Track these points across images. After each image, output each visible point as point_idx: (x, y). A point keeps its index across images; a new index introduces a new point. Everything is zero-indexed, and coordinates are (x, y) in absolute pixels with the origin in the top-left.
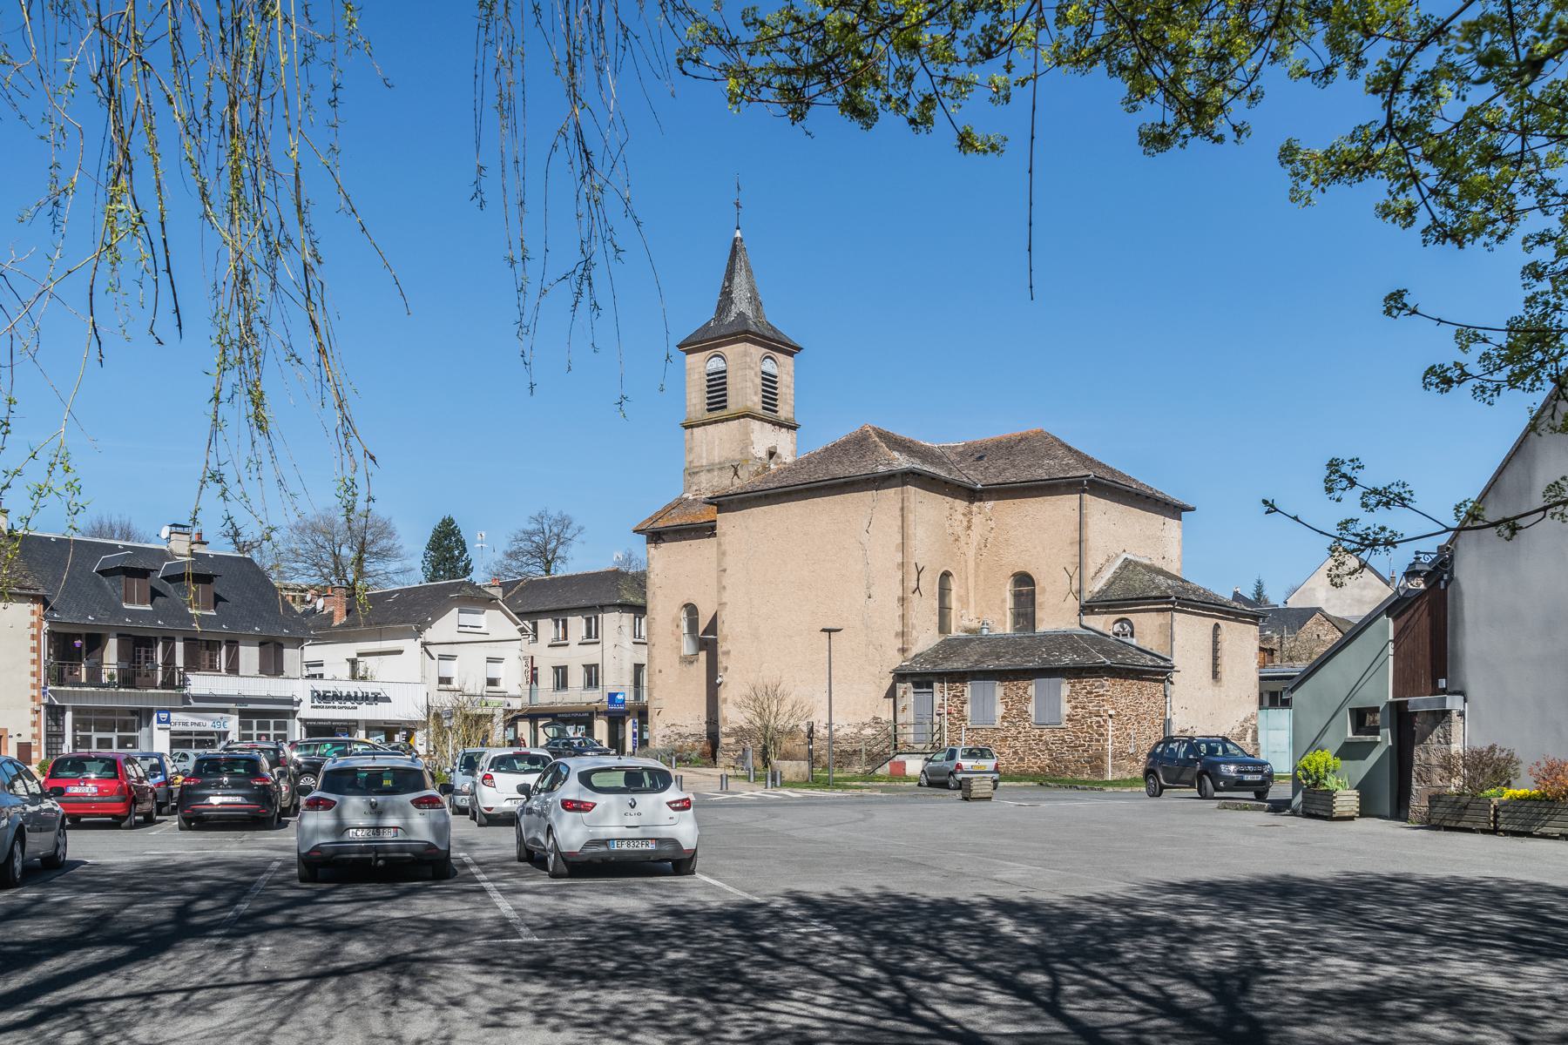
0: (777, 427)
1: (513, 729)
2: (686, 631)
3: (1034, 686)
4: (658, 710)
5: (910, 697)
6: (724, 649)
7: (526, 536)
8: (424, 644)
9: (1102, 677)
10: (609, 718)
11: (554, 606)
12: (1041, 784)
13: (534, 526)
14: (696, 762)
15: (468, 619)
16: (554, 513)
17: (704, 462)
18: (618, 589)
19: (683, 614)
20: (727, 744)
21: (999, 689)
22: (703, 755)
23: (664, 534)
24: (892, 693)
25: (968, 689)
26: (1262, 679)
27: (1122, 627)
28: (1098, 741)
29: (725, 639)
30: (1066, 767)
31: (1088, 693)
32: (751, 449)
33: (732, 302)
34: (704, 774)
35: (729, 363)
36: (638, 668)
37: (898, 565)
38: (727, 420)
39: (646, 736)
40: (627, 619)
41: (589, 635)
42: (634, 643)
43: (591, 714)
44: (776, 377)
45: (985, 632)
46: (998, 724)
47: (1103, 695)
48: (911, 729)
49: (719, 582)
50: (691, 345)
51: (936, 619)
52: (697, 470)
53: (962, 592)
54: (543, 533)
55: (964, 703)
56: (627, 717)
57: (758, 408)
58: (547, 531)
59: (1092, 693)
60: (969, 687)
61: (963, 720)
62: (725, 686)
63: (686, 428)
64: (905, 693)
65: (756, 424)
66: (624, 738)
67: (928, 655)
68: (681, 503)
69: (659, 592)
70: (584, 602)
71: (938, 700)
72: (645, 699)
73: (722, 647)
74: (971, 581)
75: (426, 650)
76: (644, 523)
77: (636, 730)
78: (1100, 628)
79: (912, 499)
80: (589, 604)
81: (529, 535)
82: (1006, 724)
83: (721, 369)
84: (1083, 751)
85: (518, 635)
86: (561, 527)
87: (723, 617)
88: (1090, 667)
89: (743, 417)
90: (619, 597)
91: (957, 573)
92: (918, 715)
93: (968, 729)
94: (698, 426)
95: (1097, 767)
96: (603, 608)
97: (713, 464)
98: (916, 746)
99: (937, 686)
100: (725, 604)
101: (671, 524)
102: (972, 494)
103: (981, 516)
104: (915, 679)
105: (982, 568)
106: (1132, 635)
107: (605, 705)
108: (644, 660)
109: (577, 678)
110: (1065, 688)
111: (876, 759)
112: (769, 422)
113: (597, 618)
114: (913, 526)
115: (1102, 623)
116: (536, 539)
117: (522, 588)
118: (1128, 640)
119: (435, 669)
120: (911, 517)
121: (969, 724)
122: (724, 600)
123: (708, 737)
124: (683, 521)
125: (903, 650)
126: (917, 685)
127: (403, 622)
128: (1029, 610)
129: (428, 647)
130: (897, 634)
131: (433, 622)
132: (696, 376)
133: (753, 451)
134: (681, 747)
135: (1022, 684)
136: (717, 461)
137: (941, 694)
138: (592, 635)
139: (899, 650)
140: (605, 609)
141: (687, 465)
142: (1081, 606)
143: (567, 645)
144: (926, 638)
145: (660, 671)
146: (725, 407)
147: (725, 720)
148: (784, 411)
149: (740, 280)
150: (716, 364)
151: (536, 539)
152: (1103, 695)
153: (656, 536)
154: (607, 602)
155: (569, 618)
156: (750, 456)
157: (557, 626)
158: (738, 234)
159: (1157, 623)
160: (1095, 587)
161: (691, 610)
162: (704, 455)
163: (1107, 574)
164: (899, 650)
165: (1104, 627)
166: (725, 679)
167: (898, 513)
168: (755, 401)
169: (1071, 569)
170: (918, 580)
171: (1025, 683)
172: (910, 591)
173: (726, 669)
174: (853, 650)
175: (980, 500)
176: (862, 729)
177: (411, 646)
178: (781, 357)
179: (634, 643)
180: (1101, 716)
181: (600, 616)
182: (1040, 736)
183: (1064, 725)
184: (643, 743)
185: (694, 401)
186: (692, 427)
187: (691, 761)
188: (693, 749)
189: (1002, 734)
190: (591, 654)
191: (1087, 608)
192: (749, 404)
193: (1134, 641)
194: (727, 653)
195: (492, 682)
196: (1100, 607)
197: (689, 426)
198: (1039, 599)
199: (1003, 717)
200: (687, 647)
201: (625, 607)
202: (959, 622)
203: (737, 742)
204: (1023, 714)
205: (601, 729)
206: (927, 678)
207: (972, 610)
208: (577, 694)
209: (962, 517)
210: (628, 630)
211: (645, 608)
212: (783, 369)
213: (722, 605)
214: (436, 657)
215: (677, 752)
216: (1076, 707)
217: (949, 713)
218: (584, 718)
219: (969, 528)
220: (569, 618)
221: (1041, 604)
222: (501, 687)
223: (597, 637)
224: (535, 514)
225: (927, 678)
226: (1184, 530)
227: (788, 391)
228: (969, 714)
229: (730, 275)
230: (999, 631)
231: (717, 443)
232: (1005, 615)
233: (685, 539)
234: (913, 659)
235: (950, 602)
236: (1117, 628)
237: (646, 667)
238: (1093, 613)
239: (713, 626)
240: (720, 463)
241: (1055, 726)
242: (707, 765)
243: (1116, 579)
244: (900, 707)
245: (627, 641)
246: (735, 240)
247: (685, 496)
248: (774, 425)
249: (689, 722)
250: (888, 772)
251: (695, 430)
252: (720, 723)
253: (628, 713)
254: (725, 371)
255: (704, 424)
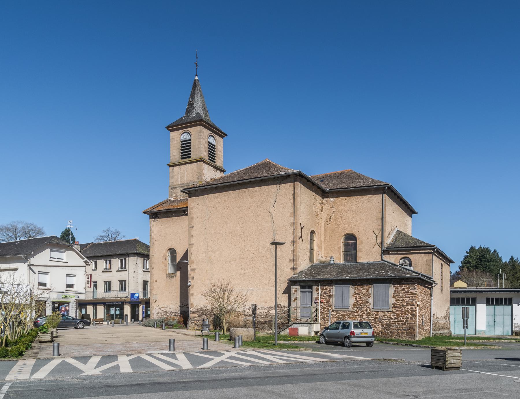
0: (215, 169)
1: (85, 309)
2: (170, 262)
3: (373, 288)
4: (155, 300)
5: (299, 293)
6: (192, 268)
7: (101, 238)
8: (30, 266)
9: (415, 284)
10: (131, 305)
11: (105, 254)
12: (382, 342)
13: (105, 234)
14: (176, 326)
15: (54, 254)
16: (113, 230)
17: (179, 183)
18: (136, 247)
19: (169, 254)
20: (193, 317)
21: (352, 290)
22: (179, 322)
23: (159, 214)
24: (287, 291)
25: (333, 290)
26: (451, 291)
27: (404, 261)
28: (412, 319)
29: (193, 262)
30: (392, 333)
31: (406, 292)
32: (203, 177)
33: (194, 108)
34: (182, 334)
35: (192, 136)
36: (145, 283)
37: (291, 223)
38: (191, 163)
39: (149, 313)
40: (140, 260)
41: (122, 267)
42: (144, 271)
43: (122, 303)
44: (215, 146)
45: (332, 262)
46: (351, 308)
47: (415, 294)
48: (299, 311)
49: (190, 233)
50: (172, 127)
51: (308, 254)
52: (176, 186)
53: (319, 243)
54: (109, 237)
55: (330, 297)
56: (140, 304)
57: (207, 158)
58: (110, 236)
59: (408, 292)
60: (334, 288)
61: (330, 306)
62: (193, 287)
63: (170, 166)
64: (296, 291)
65: (205, 166)
66: (138, 314)
67: (305, 272)
68: (167, 201)
69: (156, 243)
70: (119, 252)
71: (315, 295)
72: (149, 296)
73: (191, 267)
74: (323, 237)
75: (31, 269)
76: (149, 209)
77: (144, 310)
78: (392, 261)
79: (299, 189)
80: (122, 253)
81: (103, 237)
82: (355, 309)
83: (188, 139)
84: (402, 324)
85: (84, 264)
86: (116, 235)
87: (192, 251)
88: (407, 278)
89: (199, 161)
90: (136, 250)
91: (317, 232)
92: (302, 303)
93: (333, 311)
94: (176, 165)
95: (411, 333)
96: (128, 255)
97: (184, 184)
98: (302, 320)
99: (314, 287)
100: (193, 244)
101: (162, 209)
102: (324, 194)
103: (328, 205)
104: (302, 284)
105: (328, 231)
106: (410, 265)
107: (129, 299)
108: (148, 279)
109: (115, 286)
110: (392, 290)
111: (281, 327)
112: (212, 166)
113: (125, 260)
114: (299, 204)
115: (394, 259)
116: (106, 239)
117: (90, 247)
118: (408, 268)
119: (35, 279)
120: (298, 199)
121: (333, 308)
122: (192, 242)
123: (180, 314)
124: (169, 208)
125: (294, 269)
126: (302, 287)
127: (18, 254)
128: (353, 253)
129: (32, 267)
130: (290, 260)
131: (35, 254)
132: (175, 142)
133: (204, 178)
134: (167, 318)
135: (366, 287)
136: (186, 182)
137: (317, 292)
138: (123, 267)
139: (291, 269)
140: (130, 255)
141: (170, 184)
142: (382, 251)
143: (111, 271)
144: (304, 265)
145: (156, 281)
146: (190, 157)
147: (192, 304)
148: (219, 162)
149: (198, 99)
150: (186, 137)
151: (106, 239)
152: (415, 294)
153: (154, 215)
154: (130, 252)
155: (112, 259)
156: (202, 180)
157: (106, 263)
158: (197, 78)
159: (425, 260)
160: (388, 241)
161: (173, 251)
162: (179, 180)
163: (392, 236)
164: (291, 269)
165: (395, 261)
166: (192, 283)
167: (292, 196)
168: (205, 155)
169: (377, 232)
170: (301, 232)
171: (367, 287)
172: (298, 238)
173: (193, 278)
174: (265, 268)
175: (327, 197)
176: (269, 310)
177: (22, 267)
178: (217, 137)
179: (144, 271)
180: (414, 305)
181: (127, 258)
182: (376, 315)
183: (391, 309)
184: (147, 316)
185: (174, 154)
186: (173, 166)
187: (173, 325)
188: (174, 319)
189: (353, 314)
190: (123, 276)
191: (385, 252)
192: (202, 155)
193: (412, 268)
194: (194, 270)
195: (70, 286)
196: (393, 251)
197: (172, 166)
198: (359, 247)
199: (353, 305)
200: (170, 270)
201: (139, 255)
202: (320, 257)
203: (199, 316)
204: (366, 304)
205: (127, 310)
206: (309, 284)
207: (323, 252)
208: (115, 294)
209: (319, 204)
210: (140, 265)
211: (149, 256)
212: (219, 143)
213: (191, 245)
214: (37, 273)
215: (165, 321)
216: (398, 300)
217: (321, 302)
218: (119, 304)
219: (322, 211)
220: (112, 259)
221: (360, 249)
222: (75, 288)
223: (125, 268)
224: (105, 230)
225: (309, 284)
226: (413, 222)
227: (220, 154)
228: (334, 303)
229: (193, 95)
230: (337, 261)
231: (186, 174)
232: (340, 255)
233: (170, 217)
234: (299, 273)
235: (314, 247)
236: (401, 262)
237: (149, 282)
238: (389, 254)
239: (186, 256)
240: (187, 183)
241: (385, 310)
242: (181, 328)
243: (396, 239)
244: (293, 299)
245: (140, 270)
246: (195, 80)
247: (170, 199)
248: (214, 168)
249: (171, 306)
250: (288, 333)
251: (175, 168)
252: (190, 306)
253: (140, 302)
254: (190, 140)
255: (179, 165)
